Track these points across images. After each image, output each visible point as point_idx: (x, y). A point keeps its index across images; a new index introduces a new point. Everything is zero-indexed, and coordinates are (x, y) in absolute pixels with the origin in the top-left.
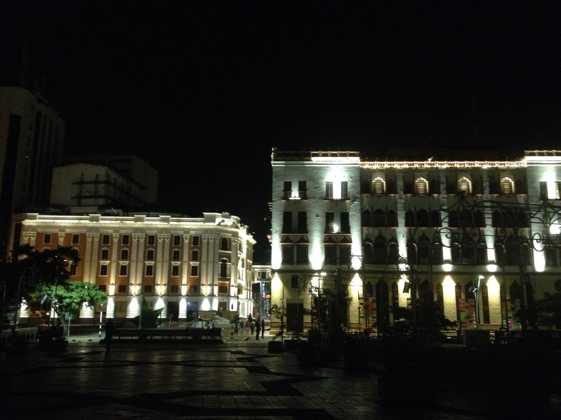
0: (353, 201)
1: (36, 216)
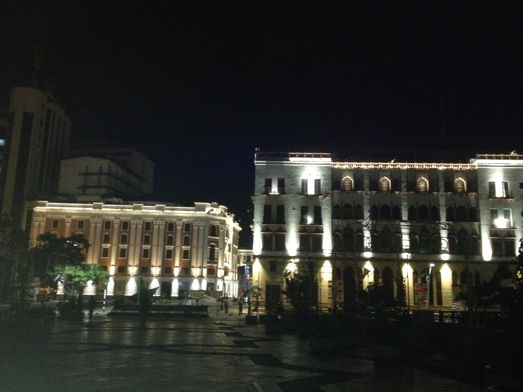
0: (325, 197)
1: (46, 203)
